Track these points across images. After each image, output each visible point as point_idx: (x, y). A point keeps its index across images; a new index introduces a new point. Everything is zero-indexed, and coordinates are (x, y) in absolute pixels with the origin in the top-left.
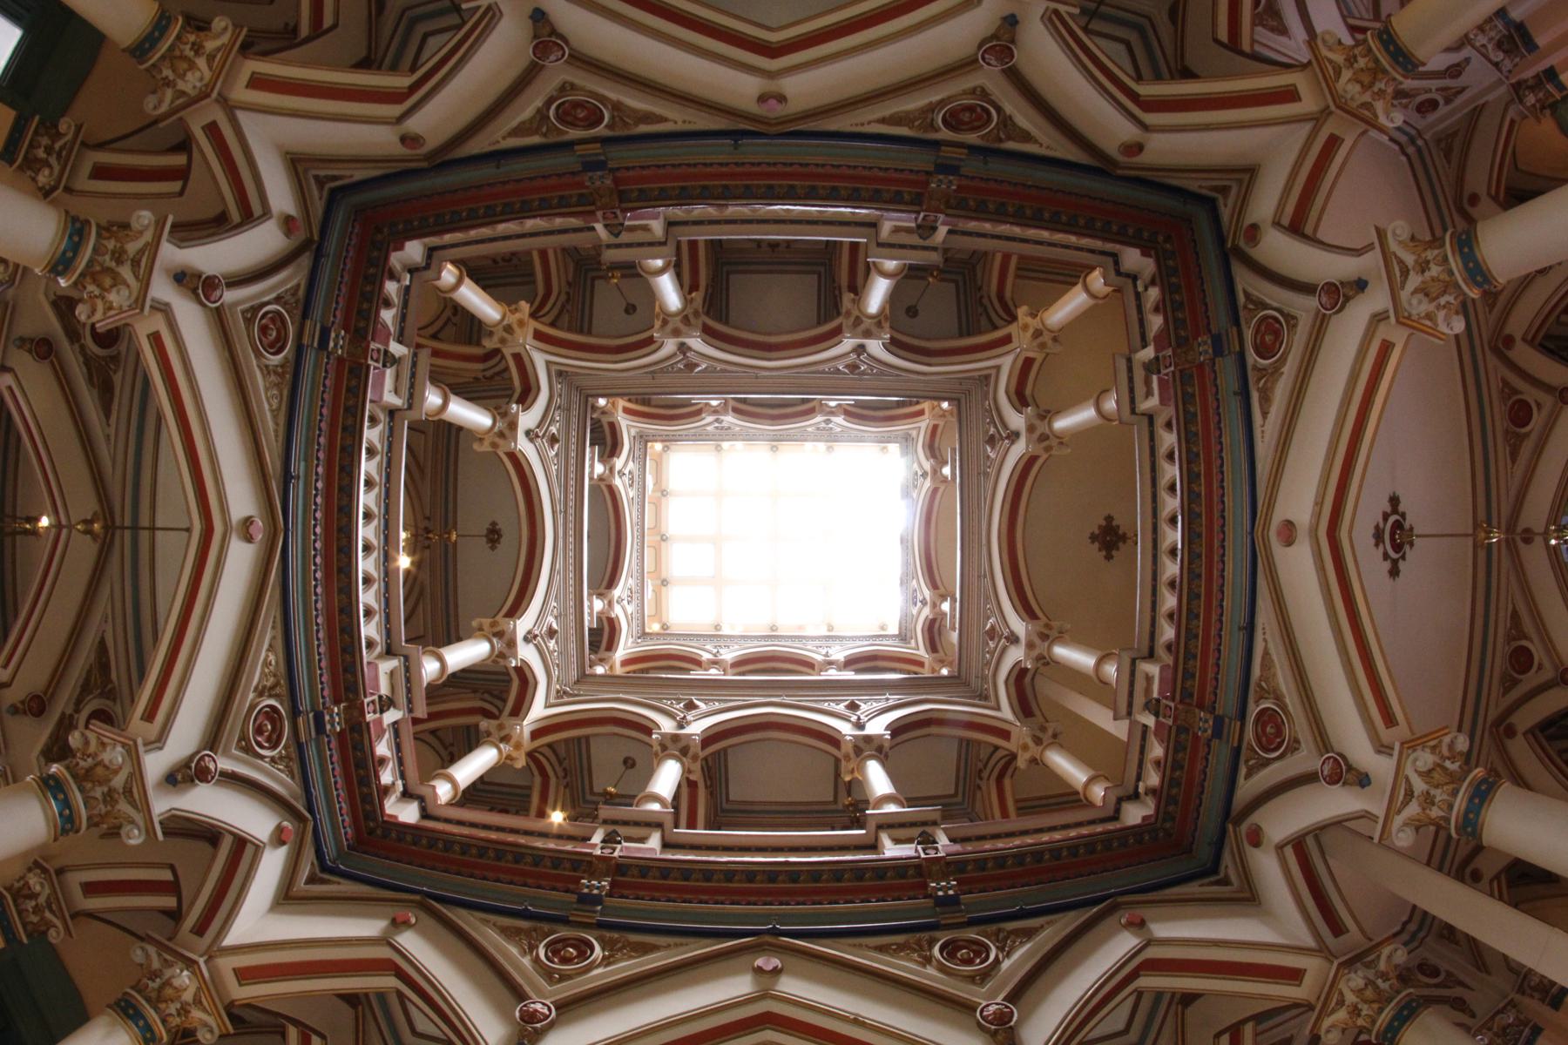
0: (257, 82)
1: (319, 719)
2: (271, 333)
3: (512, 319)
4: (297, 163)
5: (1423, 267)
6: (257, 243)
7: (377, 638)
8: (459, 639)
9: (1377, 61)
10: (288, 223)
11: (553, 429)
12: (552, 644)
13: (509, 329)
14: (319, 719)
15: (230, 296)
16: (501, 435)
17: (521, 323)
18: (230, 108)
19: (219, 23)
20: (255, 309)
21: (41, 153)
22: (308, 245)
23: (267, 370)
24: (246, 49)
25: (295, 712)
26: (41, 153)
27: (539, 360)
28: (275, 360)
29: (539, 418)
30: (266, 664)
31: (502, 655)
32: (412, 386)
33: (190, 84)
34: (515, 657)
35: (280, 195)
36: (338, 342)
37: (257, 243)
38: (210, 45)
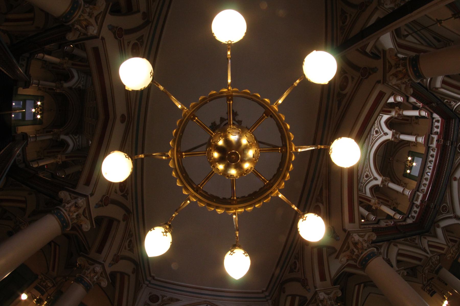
0: (443, 249)
1: (452, 145)
2: (445, 209)
3: (377, 206)
4: (436, 236)
5: (330, 299)
6: (444, 224)
7: (431, 151)
8: (41, 249)
9: (366, 250)
10: (438, 226)
11: (365, 179)
12: (377, 129)
13: (379, 204)
14: (452, 145)
15: (452, 215)
16: (386, 181)
17: (375, 204)
18: (447, 245)
19: (449, 258)
20: (447, 213)
21: (44, 284)
22: (435, 223)
23: (447, 203)
24: (445, 254)
25: (456, 147)
26: (44, 284)
27: (368, 194)
28: (444, 204)
29: (371, 183)
30: (458, 158)
31: (397, 134)
32: (414, 196)
33: (454, 249)
34: (393, 132)
35: (439, 232)
36: (432, 205)
37: (444, 224)
38: (450, 255)
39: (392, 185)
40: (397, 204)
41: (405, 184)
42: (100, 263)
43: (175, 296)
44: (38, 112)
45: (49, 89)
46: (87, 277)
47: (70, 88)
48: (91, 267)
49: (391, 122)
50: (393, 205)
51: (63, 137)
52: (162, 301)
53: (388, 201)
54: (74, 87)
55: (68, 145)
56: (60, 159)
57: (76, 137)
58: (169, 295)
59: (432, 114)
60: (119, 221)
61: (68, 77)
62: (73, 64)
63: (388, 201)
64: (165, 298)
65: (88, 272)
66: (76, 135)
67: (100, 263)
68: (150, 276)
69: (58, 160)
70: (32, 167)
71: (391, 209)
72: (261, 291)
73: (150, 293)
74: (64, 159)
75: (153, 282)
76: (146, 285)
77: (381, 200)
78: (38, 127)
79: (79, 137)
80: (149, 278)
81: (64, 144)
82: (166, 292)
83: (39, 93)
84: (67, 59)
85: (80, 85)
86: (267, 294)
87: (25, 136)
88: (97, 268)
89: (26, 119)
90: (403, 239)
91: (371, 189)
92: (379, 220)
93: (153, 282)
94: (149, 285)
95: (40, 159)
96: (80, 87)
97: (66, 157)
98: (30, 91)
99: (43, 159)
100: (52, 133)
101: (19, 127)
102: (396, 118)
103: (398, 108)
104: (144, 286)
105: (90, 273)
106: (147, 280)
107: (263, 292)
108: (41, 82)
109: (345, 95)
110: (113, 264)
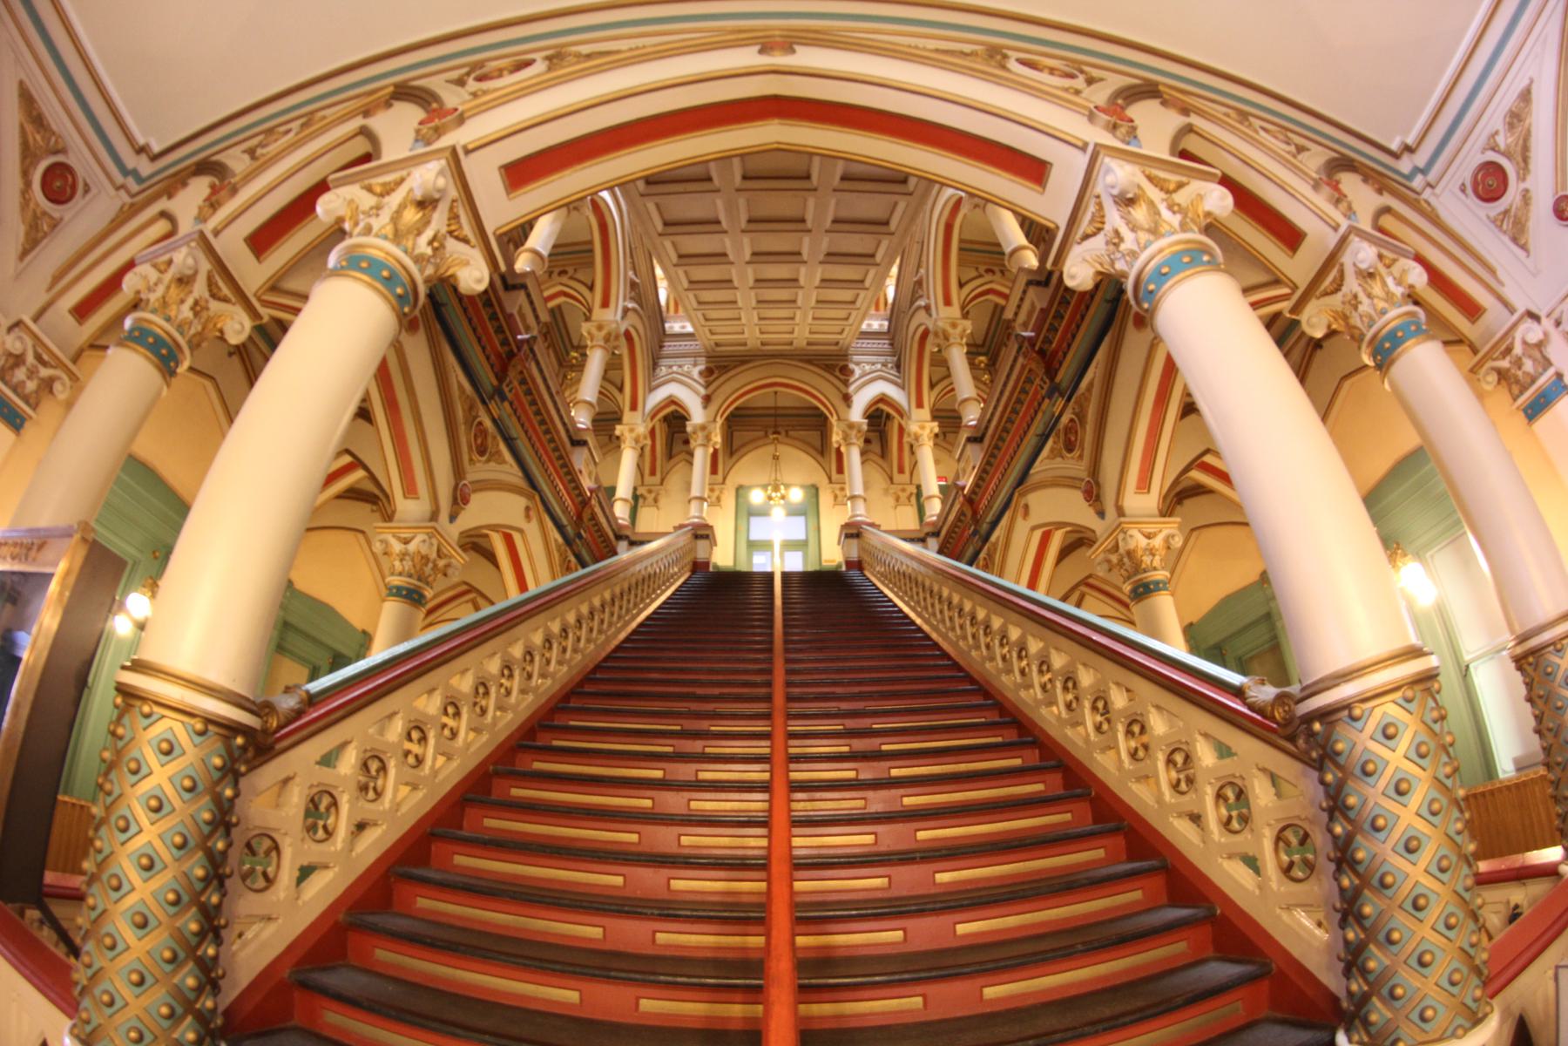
13: (637, 441)
17: (632, 430)
39: (701, 457)
40: (656, 500)
41: (718, 499)
42: (1343, 242)
43: (1506, 99)
44: (783, 497)
45: (714, 471)
46: (1383, 312)
47: (707, 400)
48: (1352, 284)
49: (888, 416)
50: (650, 492)
51: (856, 414)
52: (1507, 154)
53: (653, 473)
54: (703, 391)
55: (883, 399)
56: (921, 425)
57: (858, 372)
58: (1495, 119)
59: (936, 534)
60: (1189, 129)
61: (674, 421)
62: (634, 407)
63: (653, 473)
64: (1501, 140)
65: (1365, 306)
66: (852, 372)
67: (1343, 242)
68: (1396, 156)
69: (927, 431)
70: (939, 516)
71: (635, 489)
72: (141, 141)
73: (1463, 190)
74: (925, 413)
75: (1421, 159)
76: (1428, 190)
77: (649, 442)
78: (825, 498)
79: (858, 364)
80: (1405, 165)
81: (879, 417)
82: (1477, 130)
83: (729, 500)
84: (619, 430)
85: (695, 372)
86: (145, 167)
87: (852, 532)
88: (1361, 256)
89: (802, 536)
90: (560, 540)
91: (672, 401)
92: (584, 443)
93: (1421, 159)
94: (1431, 177)
95: (919, 494)
96: (701, 373)
97: (920, 405)
98: (723, 525)
99: (919, 487)
100: (843, 449)
101: (825, 557)
102: (901, 430)
103: (936, 430)
104: (1427, 194)
105: (1369, 296)
106: (1410, 177)
107: (141, 150)
108: (695, 492)
109: (1004, 67)
110: (1350, 208)
